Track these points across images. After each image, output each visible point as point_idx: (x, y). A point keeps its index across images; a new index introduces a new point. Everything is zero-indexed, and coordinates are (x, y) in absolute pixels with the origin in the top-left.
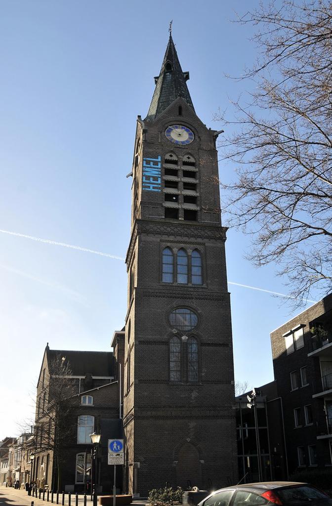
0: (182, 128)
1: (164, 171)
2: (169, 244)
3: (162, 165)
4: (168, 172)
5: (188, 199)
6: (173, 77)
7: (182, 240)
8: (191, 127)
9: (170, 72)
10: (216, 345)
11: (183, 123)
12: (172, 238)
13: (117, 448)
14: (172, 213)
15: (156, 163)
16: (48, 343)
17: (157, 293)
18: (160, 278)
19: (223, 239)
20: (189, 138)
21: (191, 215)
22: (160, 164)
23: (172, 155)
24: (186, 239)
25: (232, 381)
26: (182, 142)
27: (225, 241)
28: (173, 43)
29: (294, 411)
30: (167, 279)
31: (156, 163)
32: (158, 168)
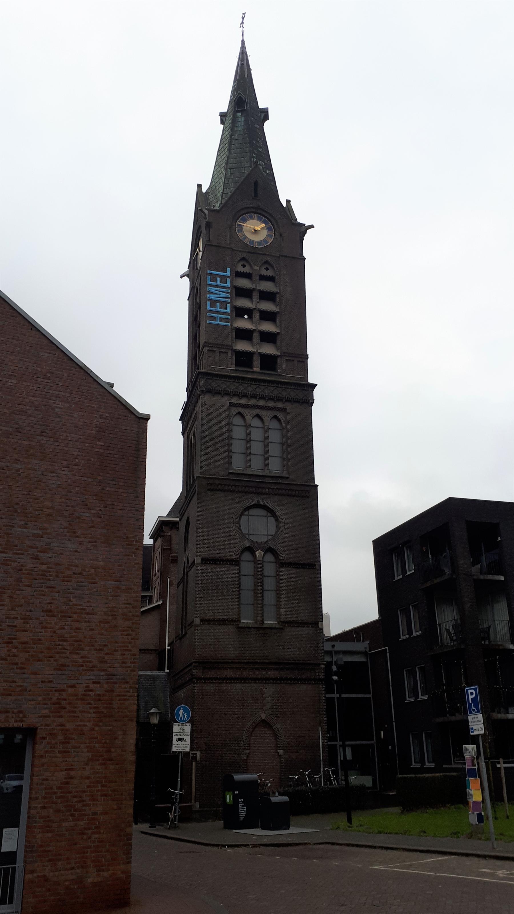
3: (232, 283)
4: (241, 292)
5: (268, 338)
9: (242, 111)
11: (259, 212)
12: (244, 401)
13: (184, 716)
14: (244, 359)
18: (230, 463)
19: (310, 402)
20: (268, 235)
21: (269, 363)
22: (229, 280)
23: (245, 264)
24: (262, 403)
25: (320, 623)
26: (258, 242)
28: (246, 54)
29: (405, 673)
31: (224, 279)
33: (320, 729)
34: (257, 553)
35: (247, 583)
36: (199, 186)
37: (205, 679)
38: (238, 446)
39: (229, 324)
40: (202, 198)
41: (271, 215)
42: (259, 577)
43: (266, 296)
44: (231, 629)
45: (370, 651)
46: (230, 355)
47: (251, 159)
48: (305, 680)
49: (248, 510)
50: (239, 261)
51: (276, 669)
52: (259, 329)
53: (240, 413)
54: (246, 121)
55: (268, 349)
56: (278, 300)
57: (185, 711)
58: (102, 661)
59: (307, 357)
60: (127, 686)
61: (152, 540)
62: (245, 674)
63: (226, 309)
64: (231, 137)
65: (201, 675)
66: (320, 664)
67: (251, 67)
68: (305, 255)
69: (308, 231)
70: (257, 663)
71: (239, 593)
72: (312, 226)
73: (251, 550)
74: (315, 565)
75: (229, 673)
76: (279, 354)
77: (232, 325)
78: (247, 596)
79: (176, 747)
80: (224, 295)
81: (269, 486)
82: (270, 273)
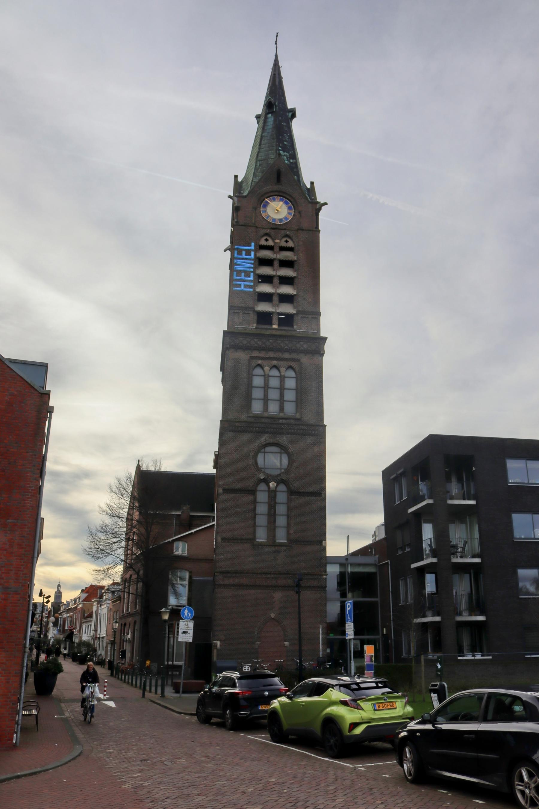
0: (281, 200)
1: (257, 262)
2: (260, 362)
3: (255, 255)
5: (286, 299)
6: (277, 115)
7: (275, 356)
8: (290, 199)
9: (272, 113)
10: (307, 491)
11: (281, 194)
14: (264, 318)
15: (248, 253)
17: (244, 427)
20: (289, 213)
21: (287, 320)
22: (253, 253)
23: (268, 238)
25: (324, 542)
27: (322, 355)
30: (257, 407)
31: (248, 253)
32: (250, 259)
34: (271, 484)
36: (236, 177)
38: (257, 394)
40: (238, 186)
41: (291, 197)
42: (272, 503)
43: (285, 264)
45: (379, 563)
47: (276, 152)
49: (264, 448)
54: (275, 121)
55: (287, 309)
59: (319, 314)
61: (215, 470)
63: (250, 277)
64: (262, 135)
67: (282, 75)
68: (320, 228)
69: (323, 208)
71: (255, 518)
72: (326, 204)
74: (321, 493)
76: (295, 312)
77: (254, 290)
78: (262, 520)
80: (249, 265)
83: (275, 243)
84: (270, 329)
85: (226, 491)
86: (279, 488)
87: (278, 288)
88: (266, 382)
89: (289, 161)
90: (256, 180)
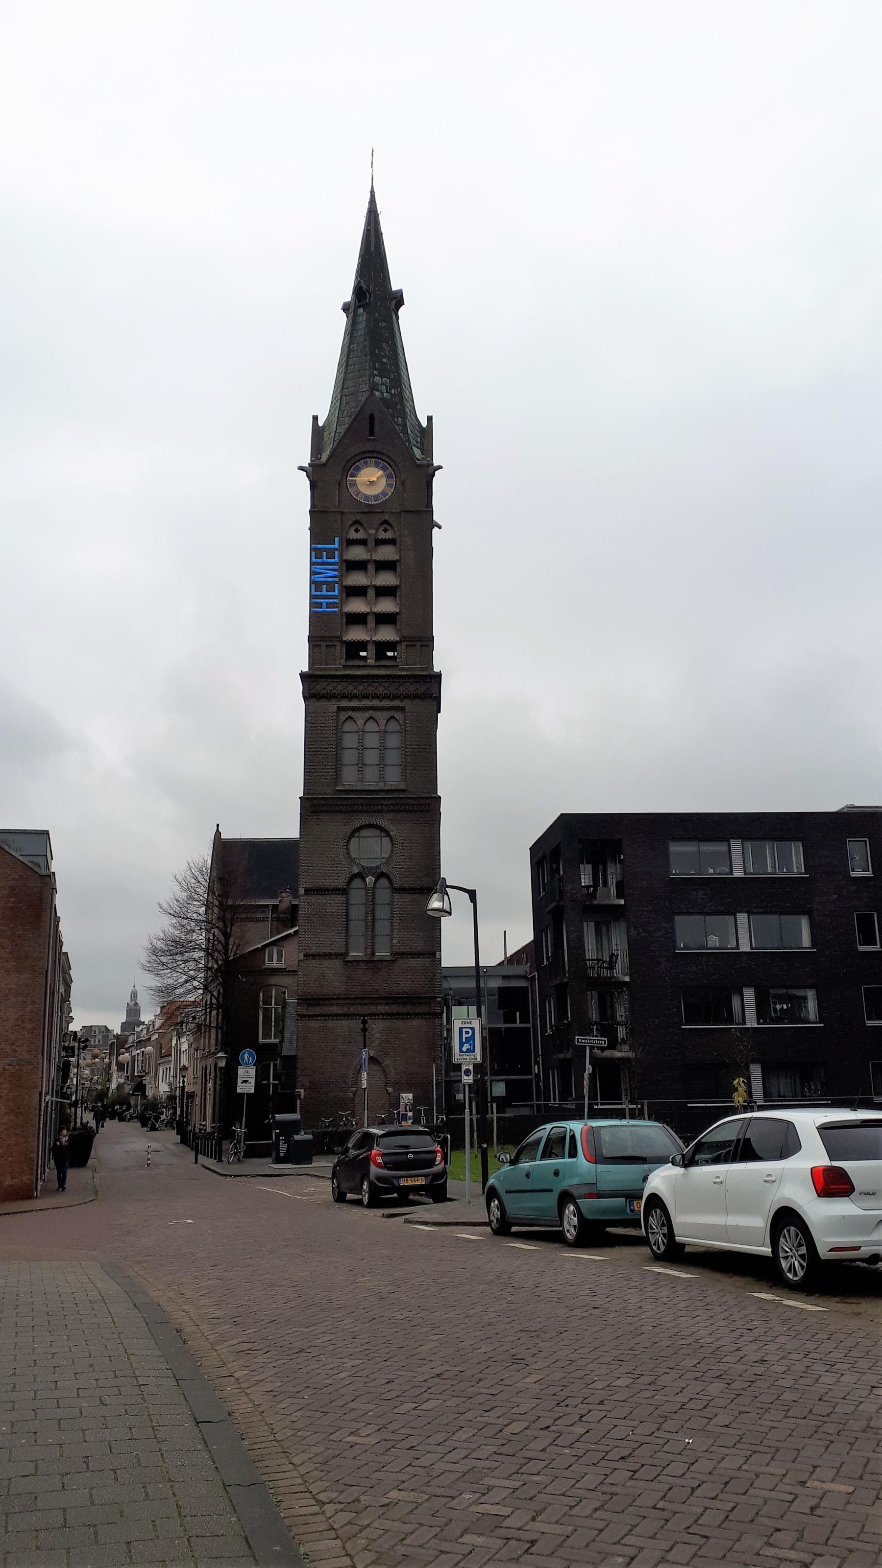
3: (341, 556)
11: (375, 455)
12: (354, 703)
16: (218, 825)
18: (337, 778)
20: (388, 485)
24: (376, 703)
25: (437, 953)
33: (434, 1066)
35: (357, 912)
36: (315, 418)
37: (309, 1016)
38: (349, 757)
39: (336, 610)
40: (318, 432)
43: (384, 566)
44: (337, 964)
46: (338, 648)
48: (418, 1014)
50: (351, 526)
51: (387, 1004)
52: (374, 610)
53: (350, 717)
55: (387, 634)
56: (398, 569)
57: (250, 1054)
58: (15, 1051)
60: (31, 1067)
62: (353, 1009)
64: (349, 347)
65: (305, 1012)
66: (436, 997)
70: (365, 998)
73: (360, 876)
75: (334, 1009)
76: (398, 639)
77: (341, 610)
78: (357, 927)
79: (241, 1088)
81: (382, 802)
82: (389, 535)
83: (370, 535)
84: (364, 666)
85: (308, 891)
86: (378, 885)
87: (375, 604)
88: (361, 741)
89: (390, 393)
90: (342, 430)
